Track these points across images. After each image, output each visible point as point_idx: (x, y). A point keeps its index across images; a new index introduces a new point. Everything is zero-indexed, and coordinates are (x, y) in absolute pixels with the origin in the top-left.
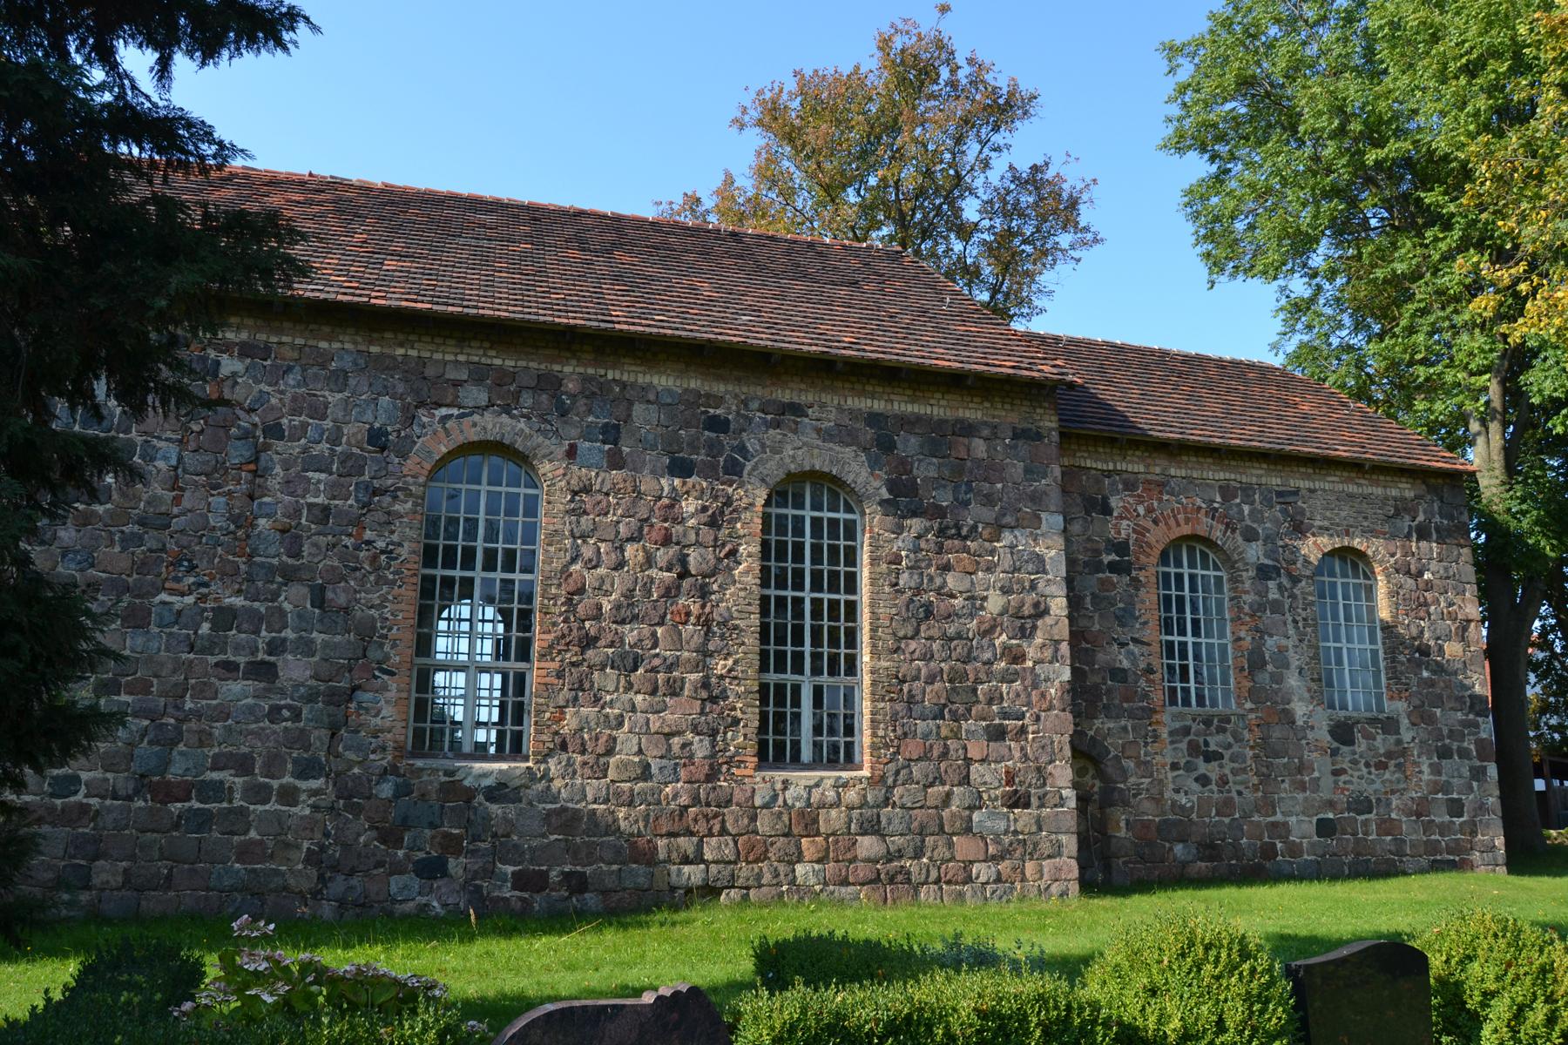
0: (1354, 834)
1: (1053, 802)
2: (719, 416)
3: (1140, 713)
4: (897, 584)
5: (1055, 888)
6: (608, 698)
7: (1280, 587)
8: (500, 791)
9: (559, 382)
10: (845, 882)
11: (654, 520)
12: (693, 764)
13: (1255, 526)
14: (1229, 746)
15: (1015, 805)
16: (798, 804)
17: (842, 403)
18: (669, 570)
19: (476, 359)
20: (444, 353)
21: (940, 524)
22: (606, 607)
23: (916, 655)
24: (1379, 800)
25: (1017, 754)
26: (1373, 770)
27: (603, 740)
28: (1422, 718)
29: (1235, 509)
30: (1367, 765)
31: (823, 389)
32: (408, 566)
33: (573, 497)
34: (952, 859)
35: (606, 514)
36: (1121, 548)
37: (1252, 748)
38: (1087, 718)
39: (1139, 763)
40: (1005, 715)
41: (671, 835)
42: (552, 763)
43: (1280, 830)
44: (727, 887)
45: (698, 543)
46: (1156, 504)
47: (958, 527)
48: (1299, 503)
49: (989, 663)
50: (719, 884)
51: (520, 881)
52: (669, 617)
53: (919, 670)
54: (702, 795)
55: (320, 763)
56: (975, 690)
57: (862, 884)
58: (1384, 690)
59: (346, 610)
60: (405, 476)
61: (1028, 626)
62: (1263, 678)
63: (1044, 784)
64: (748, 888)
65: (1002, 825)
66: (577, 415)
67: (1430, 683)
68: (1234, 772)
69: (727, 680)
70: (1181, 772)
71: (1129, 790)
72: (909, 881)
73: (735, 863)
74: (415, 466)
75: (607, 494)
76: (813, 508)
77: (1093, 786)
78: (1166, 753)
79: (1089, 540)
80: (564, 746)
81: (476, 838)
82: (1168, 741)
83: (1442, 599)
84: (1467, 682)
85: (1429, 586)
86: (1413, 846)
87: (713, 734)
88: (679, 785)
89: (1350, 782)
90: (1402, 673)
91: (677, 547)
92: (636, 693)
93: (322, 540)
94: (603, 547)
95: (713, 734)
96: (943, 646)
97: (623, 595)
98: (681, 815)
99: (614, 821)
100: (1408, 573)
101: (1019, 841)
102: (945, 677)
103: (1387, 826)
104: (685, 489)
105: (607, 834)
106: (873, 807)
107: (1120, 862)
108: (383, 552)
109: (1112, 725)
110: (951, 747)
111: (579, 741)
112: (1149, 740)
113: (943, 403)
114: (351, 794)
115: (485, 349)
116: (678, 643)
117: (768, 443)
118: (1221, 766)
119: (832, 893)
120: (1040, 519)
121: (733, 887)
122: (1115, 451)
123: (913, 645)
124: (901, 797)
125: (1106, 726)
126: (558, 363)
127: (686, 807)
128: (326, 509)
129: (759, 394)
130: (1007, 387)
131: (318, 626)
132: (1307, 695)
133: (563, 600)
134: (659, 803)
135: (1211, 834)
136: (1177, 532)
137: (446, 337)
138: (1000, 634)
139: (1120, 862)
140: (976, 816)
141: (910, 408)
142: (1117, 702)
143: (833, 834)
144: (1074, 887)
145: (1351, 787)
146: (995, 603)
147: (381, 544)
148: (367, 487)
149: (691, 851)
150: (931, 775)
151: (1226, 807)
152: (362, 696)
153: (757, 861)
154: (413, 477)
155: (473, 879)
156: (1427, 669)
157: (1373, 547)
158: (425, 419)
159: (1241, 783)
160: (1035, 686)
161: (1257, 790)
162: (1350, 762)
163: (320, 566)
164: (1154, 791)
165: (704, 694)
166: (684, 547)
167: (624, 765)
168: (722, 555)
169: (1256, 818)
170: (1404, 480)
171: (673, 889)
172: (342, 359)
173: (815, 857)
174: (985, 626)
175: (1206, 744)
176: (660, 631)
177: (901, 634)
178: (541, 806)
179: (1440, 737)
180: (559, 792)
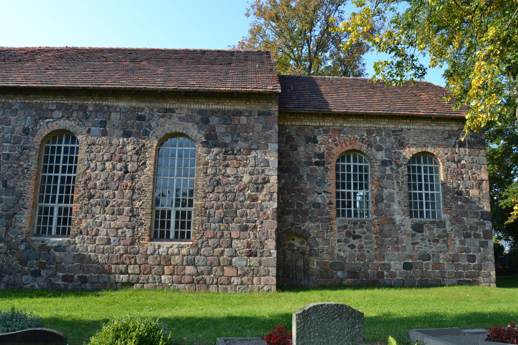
0: (421, 269)
1: (266, 255)
2: (142, 115)
3: (325, 220)
4: (206, 173)
5: (265, 288)
6: (97, 216)
7: (392, 169)
8: (59, 248)
9: (87, 107)
10: (180, 283)
11: (116, 153)
12: (126, 239)
13: (382, 145)
14: (365, 233)
15: (250, 255)
16: (163, 254)
17: (189, 107)
18: (121, 170)
19: (59, 102)
20: (49, 100)
21: (225, 150)
22: (98, 184)
23: (212, 199)
24: (434, 255)
25: (252, 236)
26: (432, 243)
27: (94, 230)
28: (457, 221)
29: (373, 138)
30: (429, 241)
31: (182, 102)
32: (33, 173)
33: (88, 147)
34: (223, 275)
35: (99, 152)
36: (321, 156)
37: (375, 234)
38: (302, 222)
39: (324, 240)
40: (248, 221)
41: (117, 264)
42: (77, 238)
43: (388, 267)
44: (136, 283)
45: (131, 161)
46: (337, 138)
47: (233, 150)
48: (403, 135)
49: (242, 201)
50: (133, 282)
51: (64, 278)
52: (120, 187)
53: (213, 204)
54: (129, 250)
55: (2, 238)
56: (236, 212)
57: (187, 284)
58: (442, 210)
59: (13, 188)
60: (34, 143)
61: (260, 187)
62: (382, 206)
63: (263, 248)
64: (144, 284)
65: (244, 263)
66: (92, 118)
67: (462, 207)
68: (366, 243)
69: (140, 209)
70: (342, 243)
71: (319, 250)
72: (205, 283)
73: (140, 274)
74: (37, 140)
75: (100, 145)
76: (424, 163)
77: (307, 248)
78: (335, 236)
79: (307, 153)
80: (81, 233)
81: (50, 264)
82: (337, 231)
83: (470, 172)
84: (481, 206)
85: (463, 166)
86: (449, 274)
87: (134, 228)
88: (120, 246)
89: (421, 248)
90: (448, 203)
91: (124, 163)
92: (107, 214)
93: (7, 165)
94: (98, 163)
95: (134, 228)
96: (223, 195)
97: (104, 180)
98: (120, 257)
99: (97, 259)
100: (454, 161)
101: (251, 270)
102: (224, 207)
103: (437, 266)
104: (128, 142)
105: (94, 263)
106: (192, 255)
107: (314, 278)
108: (25, 168)
109: (312, 225)
110: (225, 234)
111: (86, 231)
112: (329, 231)
113: (230, 104)
114: (11, 249)
115: (62, 98)
116: (123, 196)
117: (159, 123)
118: (360, 241)
119: (175, 286)
120: (268, 146)
121: (138, 283)
122: (320, 118)
123: (211, 195)
124: (204, 252)
125: (310, 225)
126: (86, 101)
127: (123, 254)
128: (8, 156)
129: (158, 106)
130: (257, 96)
131: (4, 194)
132: (402, 212)
133: (83, 182)
134: (113, 253)
135: (354, 268)
136: (346, 149)
137: (50, 95)
138: (248, 191)
139: (314, 278)
140: (234, 260)
141: (216, 107)
142: (315, 216)
143: (176, 265)
144: (274, 288)
145: (421, 250)
146: (246, 178)
147: (25, 166)
148: (21, 147)
149: (123, 270)
150: (216, 244)
151: (362, 257)
152: (17, 216)
153: (147, 274)
154: (36, 143)
155: (49, 277)
156: (460, 201)
157: (439, 152)
158: (41, 123)
159: (369, 248)
160: (262, 210)
161: (377, 250)
162: (421, 239)
163: (6, 174)
164: (330, 250)
165: (131, 214)
166: (127, 162)
167: (101, 239)
168: (140, 164)
169: (375, 262)
170: (453, 123)
171: (117, 283)
172: (16, 105)
173: (169, 273)
174: (242, 187)
175: (354, 232)
176: (116, 192)
177: (207, 191)
178: (72, 253)
179: (466, 229)
180: (79, 248)
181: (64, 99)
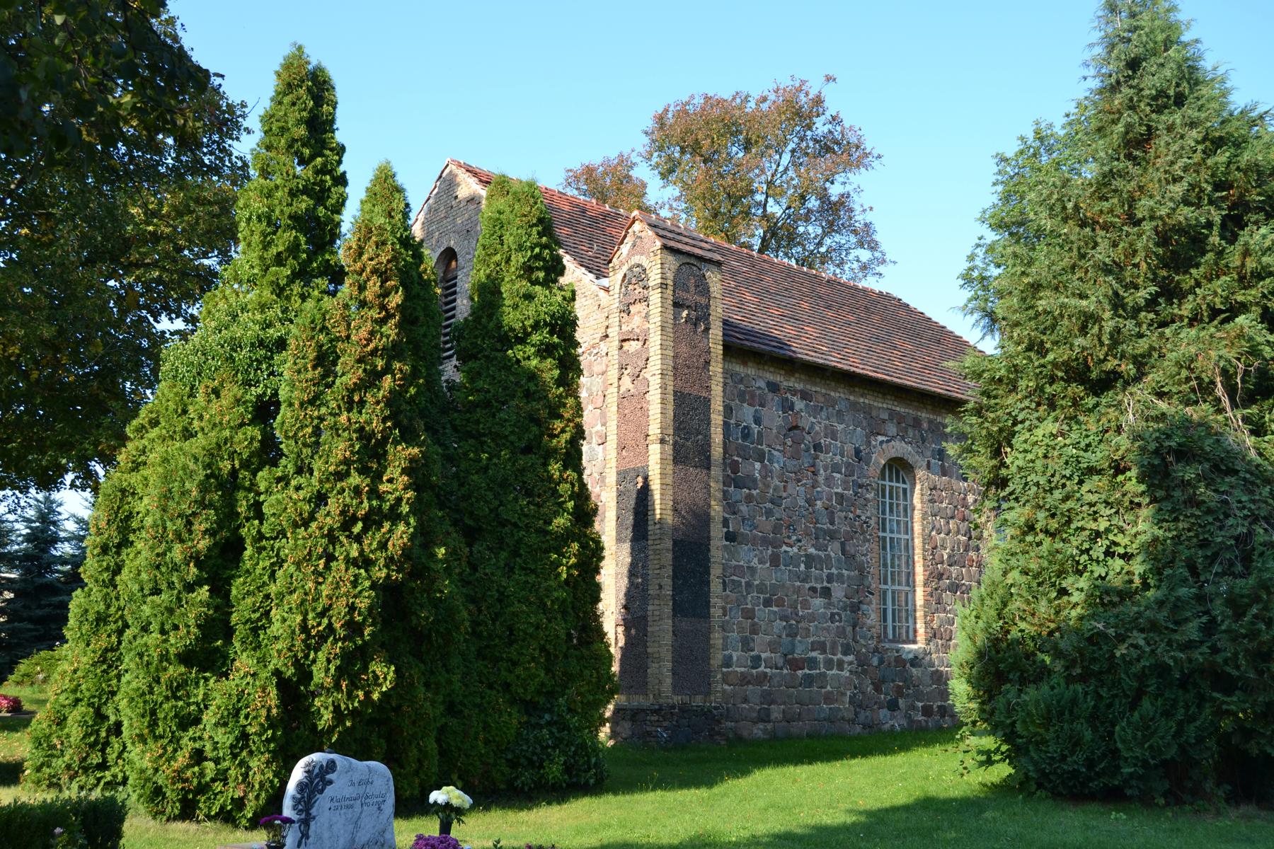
152: (864, 607)
181: (896, 403)
